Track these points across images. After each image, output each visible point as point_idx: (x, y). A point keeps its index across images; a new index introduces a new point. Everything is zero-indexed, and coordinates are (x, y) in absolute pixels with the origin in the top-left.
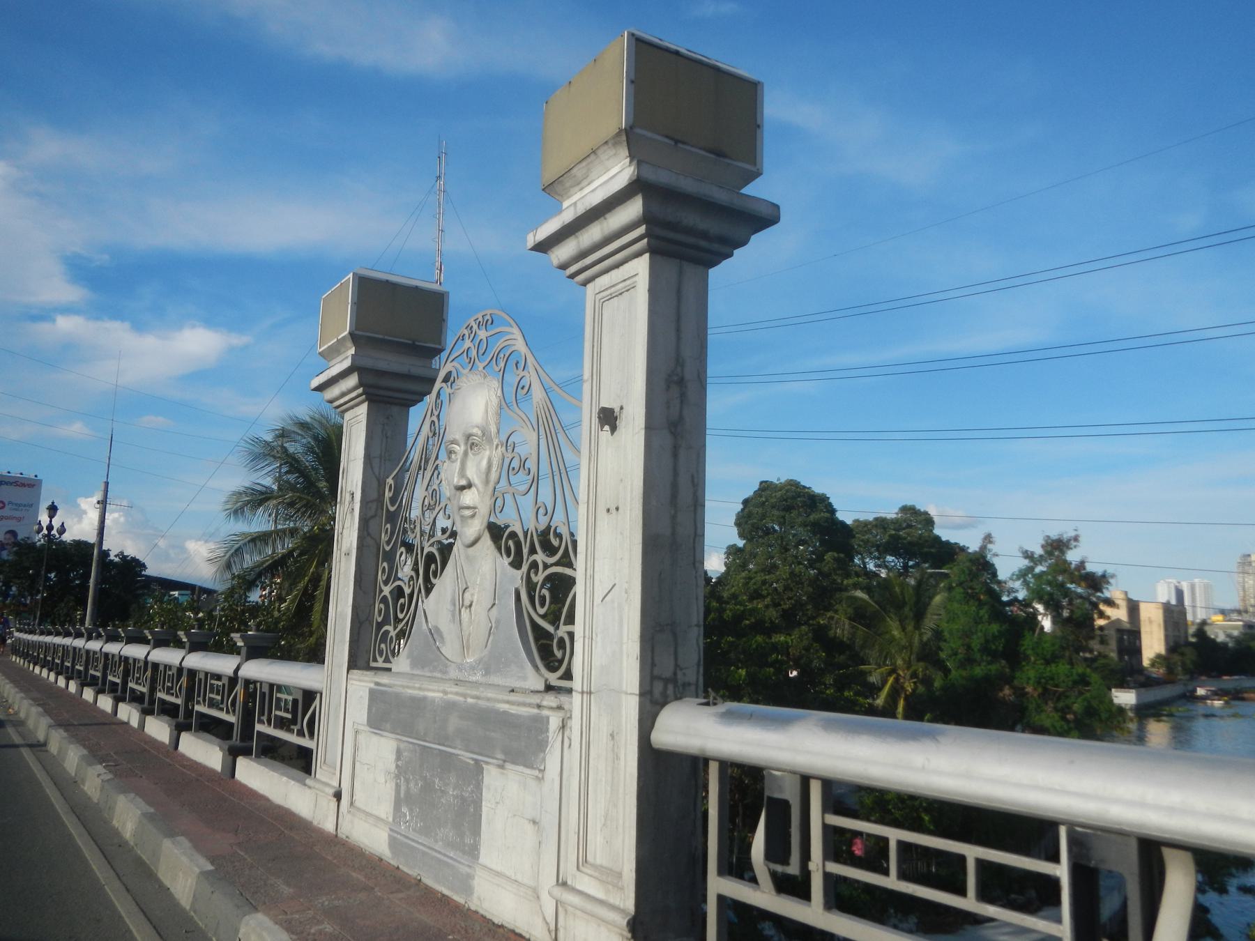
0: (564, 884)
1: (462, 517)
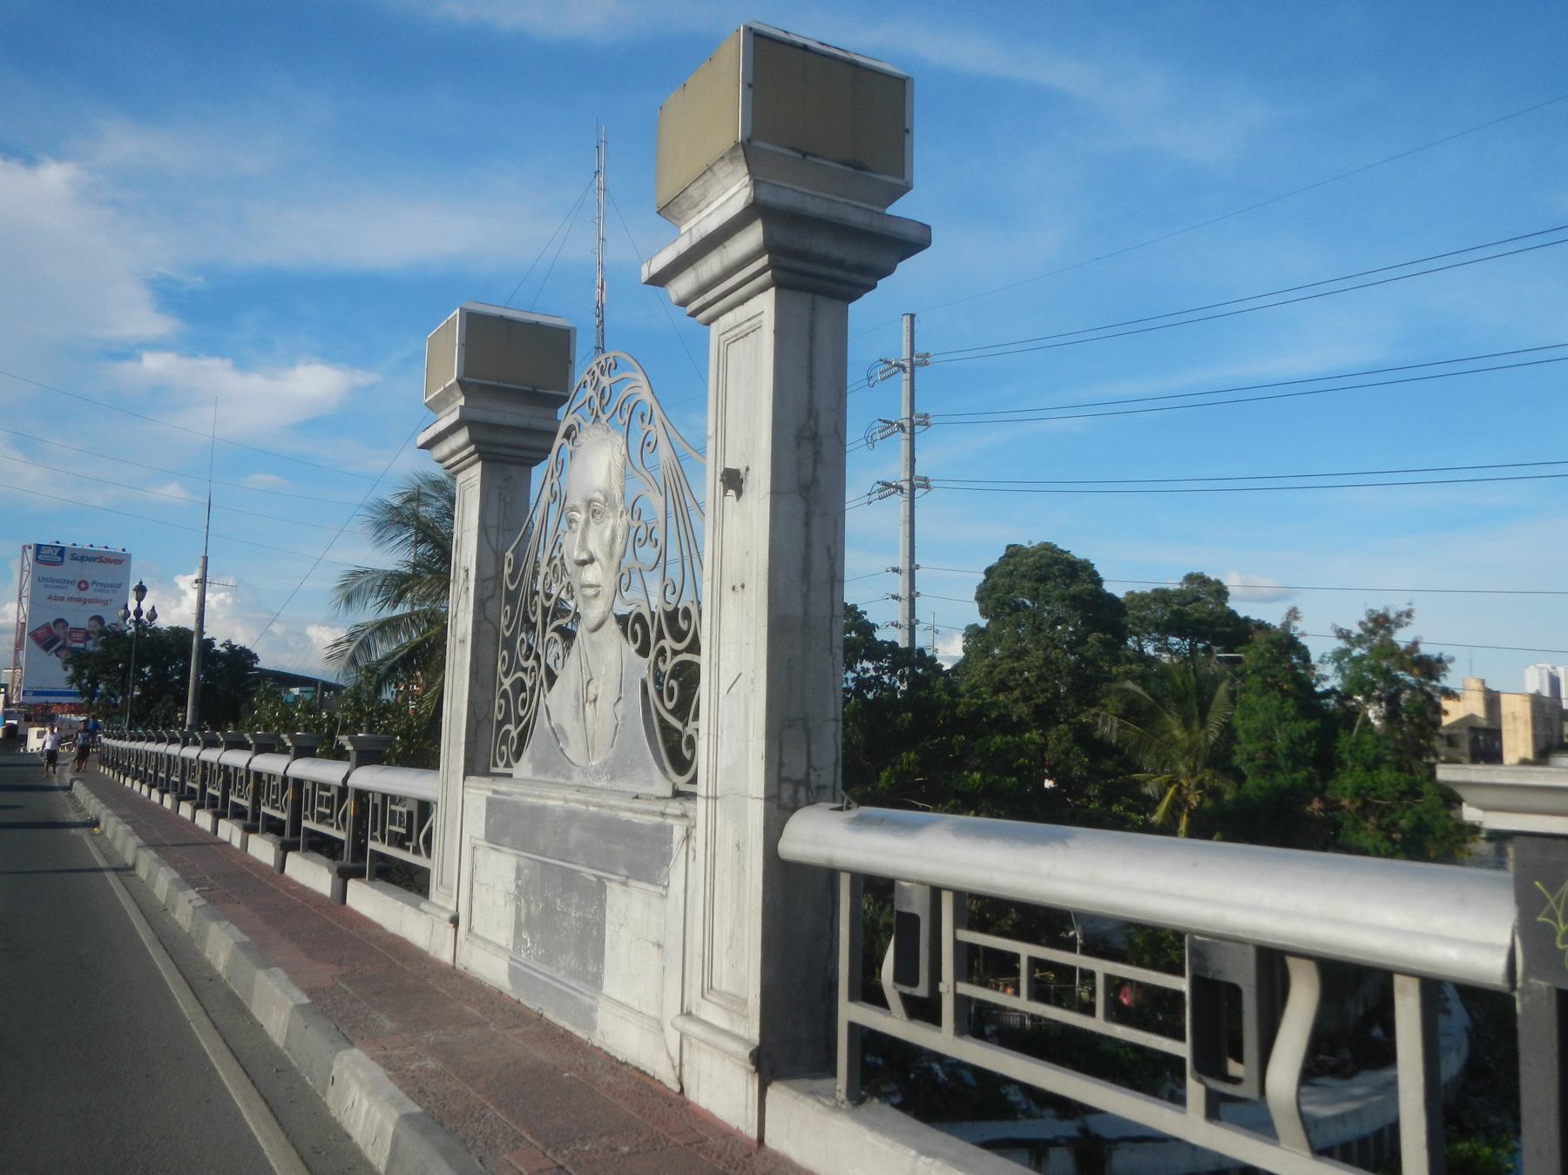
0: (689, 1014)
1: (584, 596)
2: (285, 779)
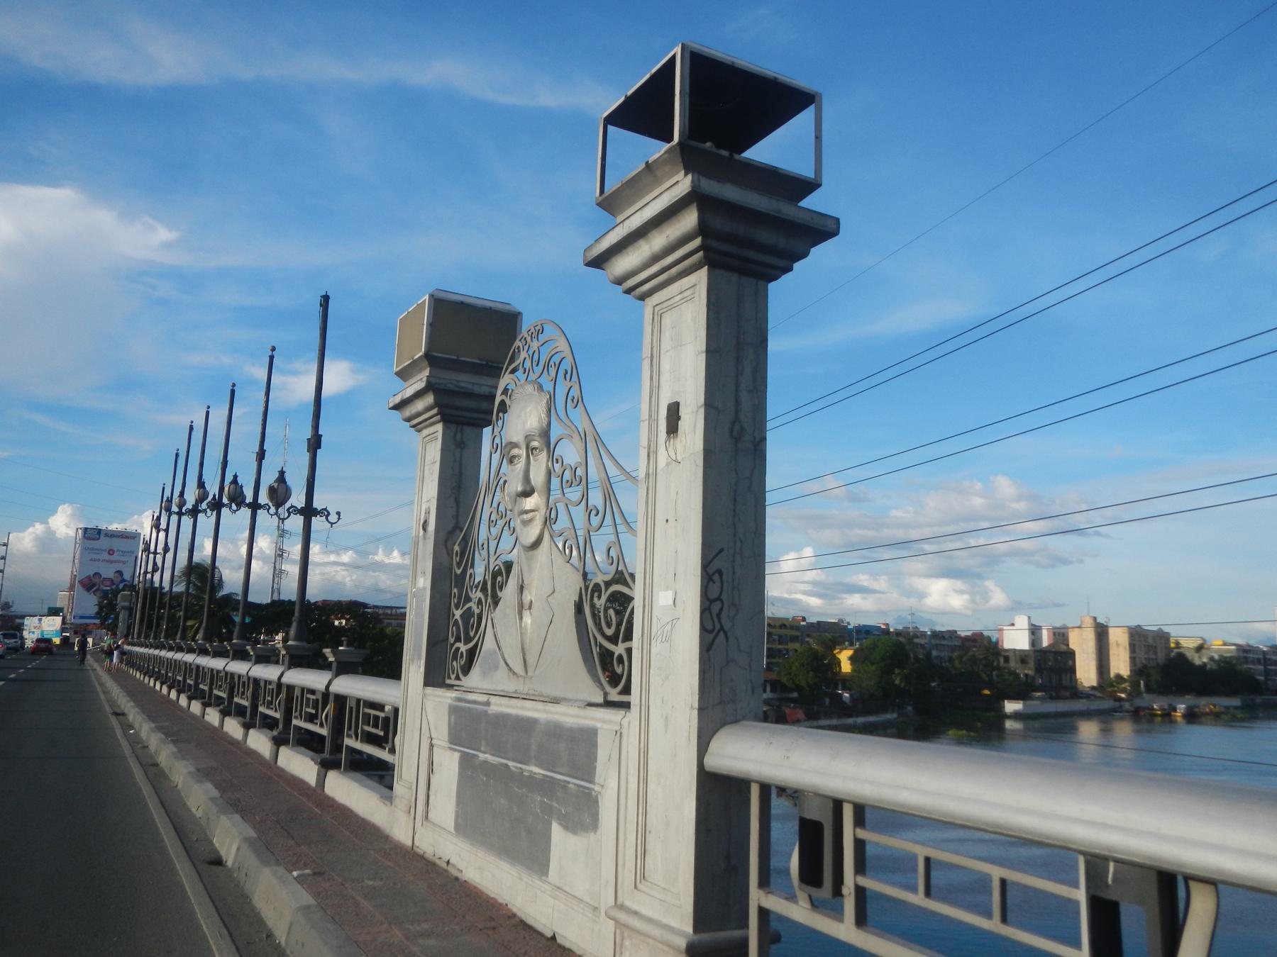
2: (279, 685)
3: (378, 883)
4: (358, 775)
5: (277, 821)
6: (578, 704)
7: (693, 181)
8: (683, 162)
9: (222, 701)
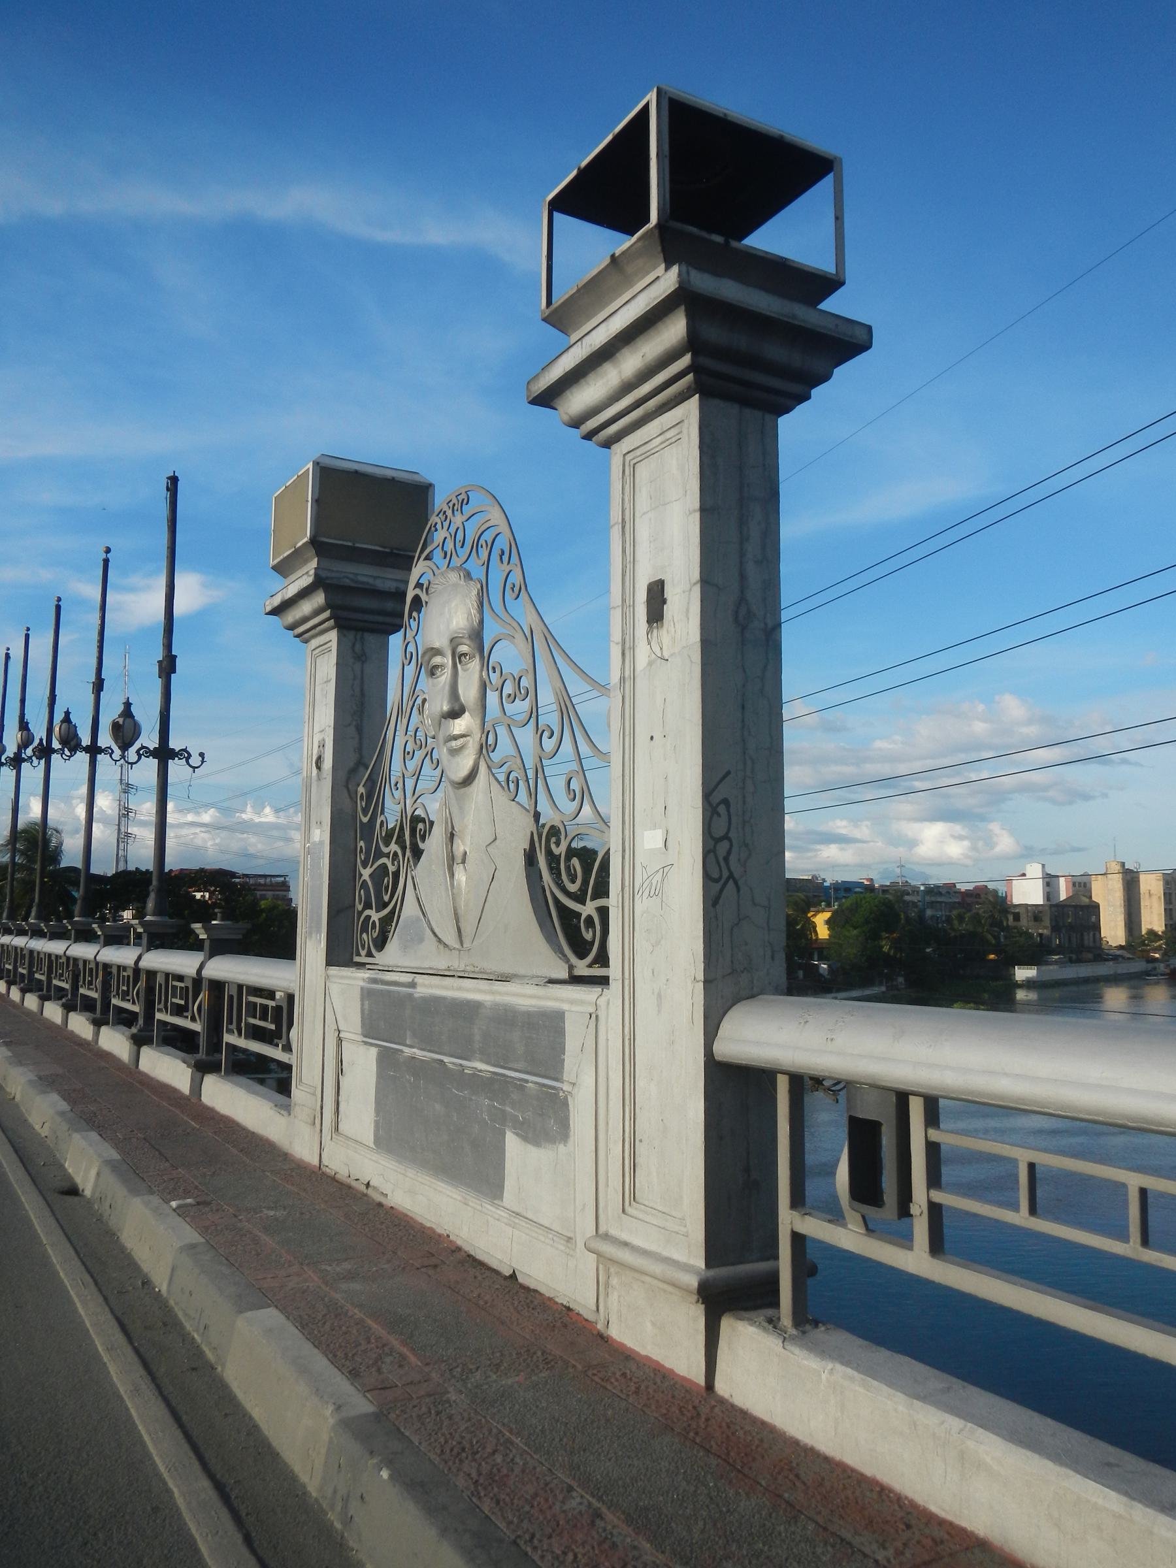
2: (137, 970)
3: (280, 1214)
4: (243, 1080)
5: (145, 1139)
6: (535, 981)
7: (680, 275)
8: (664, 251)
9: (64, 993)
